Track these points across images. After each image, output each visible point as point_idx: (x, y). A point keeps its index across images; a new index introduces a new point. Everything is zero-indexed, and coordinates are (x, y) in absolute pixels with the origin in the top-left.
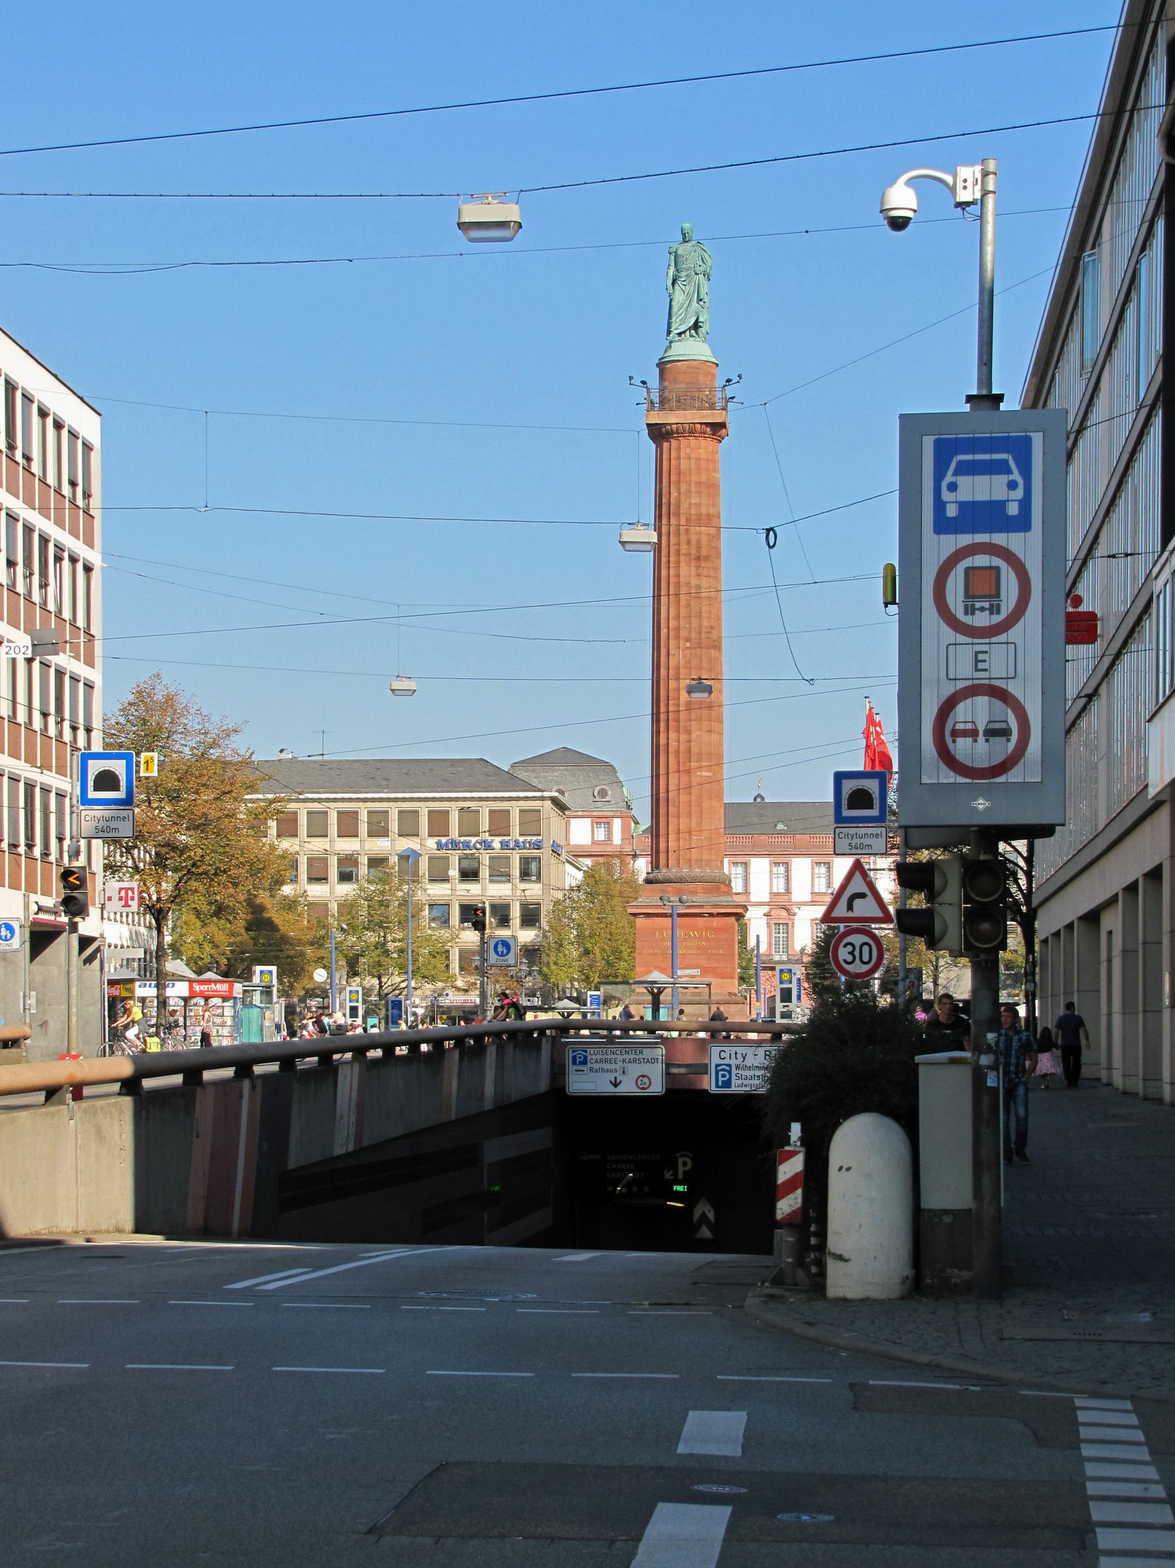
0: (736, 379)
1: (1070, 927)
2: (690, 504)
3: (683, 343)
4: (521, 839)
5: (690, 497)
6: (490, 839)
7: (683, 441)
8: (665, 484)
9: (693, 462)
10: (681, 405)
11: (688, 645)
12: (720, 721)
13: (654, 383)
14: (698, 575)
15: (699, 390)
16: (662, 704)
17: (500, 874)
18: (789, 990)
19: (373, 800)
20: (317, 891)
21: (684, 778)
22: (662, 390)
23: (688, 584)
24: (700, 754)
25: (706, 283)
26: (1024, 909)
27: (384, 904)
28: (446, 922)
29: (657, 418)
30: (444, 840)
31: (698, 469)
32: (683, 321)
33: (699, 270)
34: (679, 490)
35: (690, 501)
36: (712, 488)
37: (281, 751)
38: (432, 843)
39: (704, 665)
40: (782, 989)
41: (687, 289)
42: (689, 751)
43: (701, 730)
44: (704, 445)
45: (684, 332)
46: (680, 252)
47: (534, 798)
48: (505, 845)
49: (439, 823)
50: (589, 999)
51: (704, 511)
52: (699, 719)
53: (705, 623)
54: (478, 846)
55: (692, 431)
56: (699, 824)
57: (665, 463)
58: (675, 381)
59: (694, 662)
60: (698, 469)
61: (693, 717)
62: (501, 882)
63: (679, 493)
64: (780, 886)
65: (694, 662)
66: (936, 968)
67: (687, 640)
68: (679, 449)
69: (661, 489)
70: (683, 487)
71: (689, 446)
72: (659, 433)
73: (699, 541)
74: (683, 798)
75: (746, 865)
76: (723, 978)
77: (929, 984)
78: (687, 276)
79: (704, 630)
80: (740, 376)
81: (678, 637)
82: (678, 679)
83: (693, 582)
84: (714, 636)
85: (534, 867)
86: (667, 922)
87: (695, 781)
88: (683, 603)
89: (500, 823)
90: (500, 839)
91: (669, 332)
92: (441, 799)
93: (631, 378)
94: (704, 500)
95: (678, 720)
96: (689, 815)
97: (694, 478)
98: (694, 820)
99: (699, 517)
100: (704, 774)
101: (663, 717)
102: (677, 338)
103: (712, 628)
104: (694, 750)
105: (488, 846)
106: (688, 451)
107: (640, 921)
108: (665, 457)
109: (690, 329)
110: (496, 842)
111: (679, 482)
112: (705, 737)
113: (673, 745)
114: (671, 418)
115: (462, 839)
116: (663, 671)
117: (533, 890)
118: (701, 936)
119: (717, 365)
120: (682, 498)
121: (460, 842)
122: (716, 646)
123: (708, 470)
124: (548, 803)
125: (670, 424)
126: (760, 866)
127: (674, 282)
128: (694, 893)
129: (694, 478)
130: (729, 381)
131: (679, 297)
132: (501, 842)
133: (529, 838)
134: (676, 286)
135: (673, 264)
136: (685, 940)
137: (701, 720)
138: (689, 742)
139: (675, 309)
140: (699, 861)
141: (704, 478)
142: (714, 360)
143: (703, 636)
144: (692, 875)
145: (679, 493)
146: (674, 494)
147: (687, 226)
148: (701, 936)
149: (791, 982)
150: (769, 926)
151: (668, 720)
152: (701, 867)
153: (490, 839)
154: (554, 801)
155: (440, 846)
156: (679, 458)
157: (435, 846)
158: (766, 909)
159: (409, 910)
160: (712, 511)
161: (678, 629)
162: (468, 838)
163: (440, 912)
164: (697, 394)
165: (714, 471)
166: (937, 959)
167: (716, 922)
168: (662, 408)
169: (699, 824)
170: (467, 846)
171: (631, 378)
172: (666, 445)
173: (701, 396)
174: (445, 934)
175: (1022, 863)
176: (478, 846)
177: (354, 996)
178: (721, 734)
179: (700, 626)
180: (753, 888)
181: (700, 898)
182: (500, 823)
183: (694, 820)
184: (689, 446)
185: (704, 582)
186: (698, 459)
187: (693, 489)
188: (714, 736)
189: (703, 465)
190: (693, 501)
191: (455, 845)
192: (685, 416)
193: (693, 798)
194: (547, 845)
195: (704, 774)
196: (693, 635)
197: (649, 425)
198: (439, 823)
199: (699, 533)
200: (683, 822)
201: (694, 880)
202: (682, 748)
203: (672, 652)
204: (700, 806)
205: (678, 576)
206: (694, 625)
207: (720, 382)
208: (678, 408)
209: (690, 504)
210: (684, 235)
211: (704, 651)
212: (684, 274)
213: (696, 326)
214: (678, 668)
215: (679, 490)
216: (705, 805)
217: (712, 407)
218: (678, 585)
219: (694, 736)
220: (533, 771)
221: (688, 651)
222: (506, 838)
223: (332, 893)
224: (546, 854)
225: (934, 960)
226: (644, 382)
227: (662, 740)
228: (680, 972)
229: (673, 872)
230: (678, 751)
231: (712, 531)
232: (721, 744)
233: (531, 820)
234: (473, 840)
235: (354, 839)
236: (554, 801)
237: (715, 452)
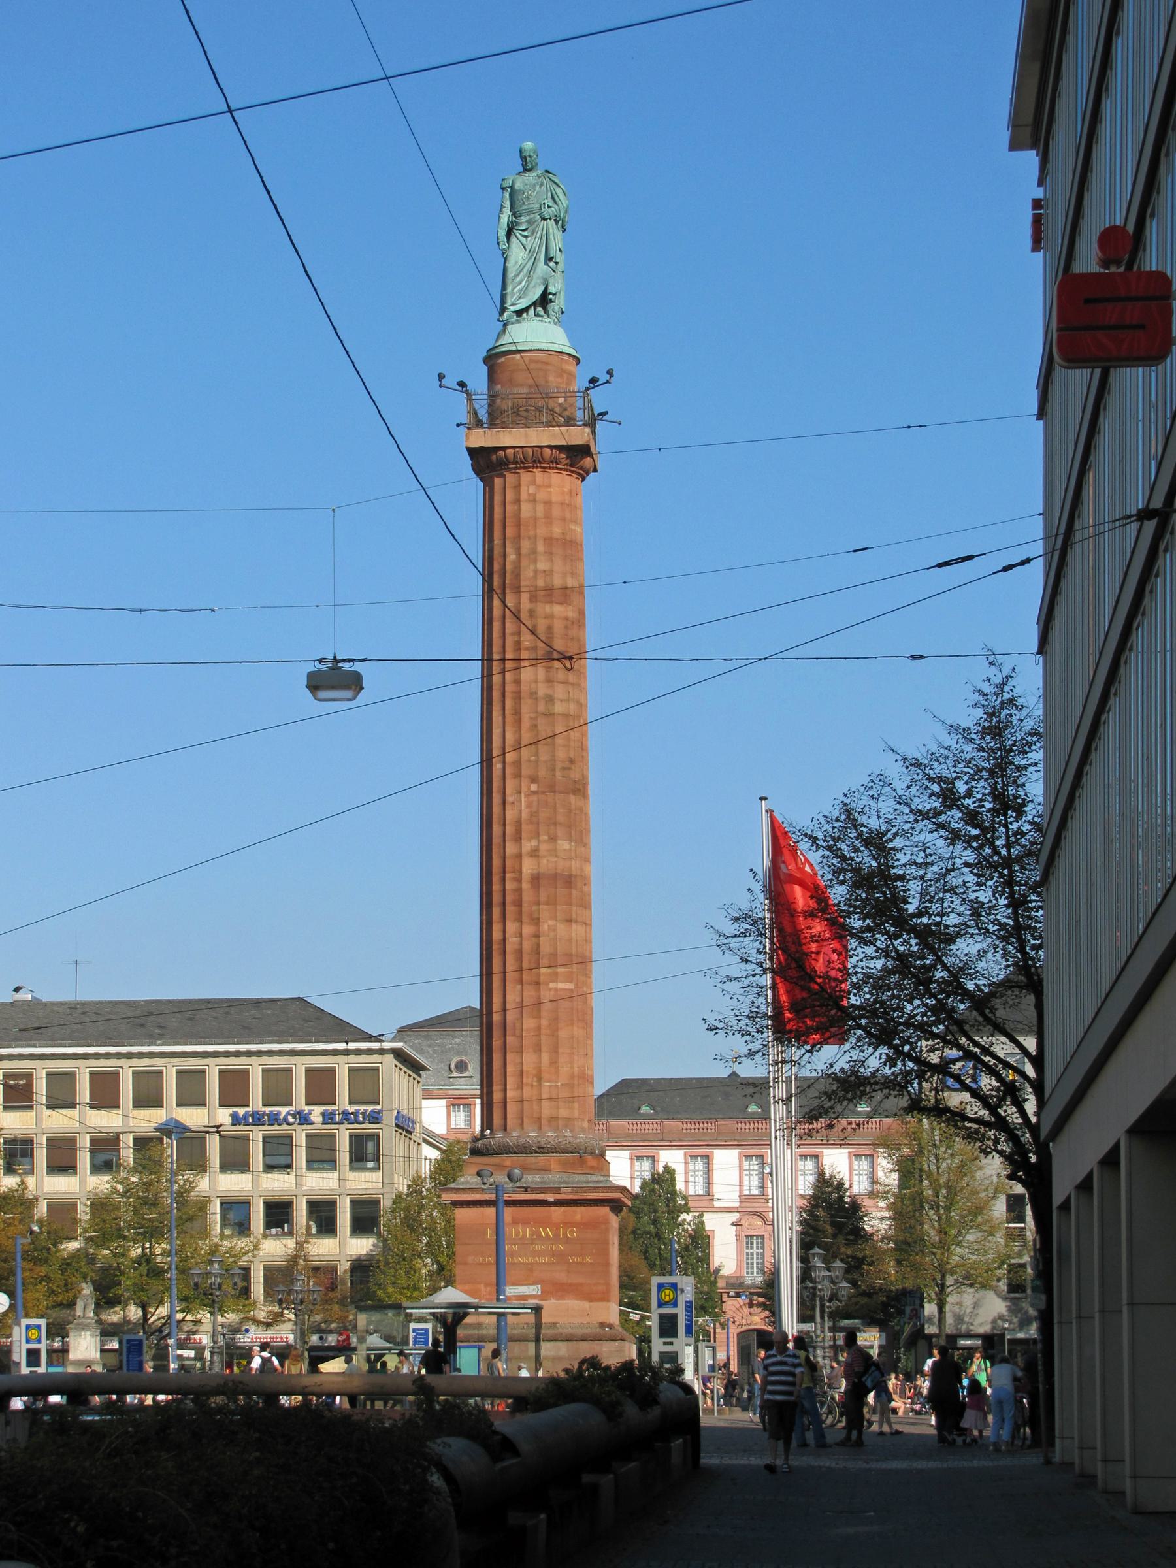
0: (603, 377)
1: (1110, 1160)
2: (536, 571)
3: (524, 325)
4: (352, 1109)
5: (535, 561)
6: (307, 1109)
7: (525, 477)
8: (497, 541)
9: (540, 508)
10: (521, 418)
11: (534, 787)
12: (586, 905)
13: (479, 381)
14: (549, 681)
15: (548, 396)
16: (496, 879)
17: (322, 1155)
18: (673, 1318)
19: (140, 1055)
20: (61, 1186)
21: (529, 994)
22: (493, 397)
23: (533, 695)
24: (554, 955)
25: (559, 234)
26: (1033, 1158)
27: (154, 1203)
28: (243, 1228)
29: (482, 439)
30: (241, 1111)
31: (548, 517)
32: (524, 293)
33: (547, 212)
34: (518, 551)
35: (538, 567)
36: (571, 548)
37: (17, 990)
38: (224, 1116)
39: (561, 818)
40: (661, 1316)
41: (529, 242)
42: (537, 950)
43: (555, 918)
44: (559, 483)
45: (526, 310)
46: (518, 186)
47: (370, 1052)
48: (328, 1118)
49: (234, 1088)
50: (411, 1335)
51: (557, 582)
52: (552, 902)
53: (561, 754)
54: (291, 1119)
55: (535, 459)
56: (554, 1063)
57: (497, 510)
58: (511, 382)
59: (543, 815)
60: (548, 517)
61: (543, 898)
62: (323, 1169)
63: (519, 555)
64: (752, 1185)
65: (543, 815)
66: (942, 1287)
67: (534, 780)
68: (517, 487)
69: (491, 550)
70: (525, 545)
71: (533, 483)
72: (487, 463)
73: (550, 628)
74: (529, 1023)
75: (707, 1159)
76: (591, 1300)
77: (930, 1309)
78: (528, 222)
79: (559, 765)
80: (610, 373)
81: (518, 776)
82: (518, 838)
83: (542, 690)
84: (575, 775)
85: (370, 1146)
86: (491, 1212)
87: (546, 995)
88: (526, 724)
89: (321, 1086)
90: (322, 1109)
91: (503, 310)
92: (238, 1054)
93: (441, 377)
94: (558, 565)
95: (519, 904)
96: (538, 1049)
97: (542, 531)
98: (545, 1057)
99: (550, 590)
100: (561, 985)
101: (496, 898)
102: (515, 318)
103: (572, 761)
104: (545, 949)
105: (304, 1119)
106: (532, 490)
107: (462, 1214)
108: (497, 498)
109: (534, 304)
110: (316, 1113)
111: (518, 538)
112: (562, 929)
113: (512, 942)
114: (509, 438)
115: (267, 1109)
116: (496, 828)
117: (366, 1182)
118: (556, 1235)
119: (578, 361)
120: (524, 563)
121: (264, 1114)
122: (579, 789)
123: (564, 519)
124: (390, 1059)
125: (504, 449)
126: (726, 1159)
127: (509, 234)
128: (546, 1170)
129: (542, 531)
130: (593, 381)
131: (517, 255)
132: (323, 1114)
133: (362, 1108)
134: (513, 239)
135: (507, 204)
136: (532, 1242)
137: (555, 904)
138: (537, 936)
139: (511, 274)
140: (554, 1119)
141: (557, 530)
142: (572, 352)
143: (558, 774)
144: (543, 1141)
145: (519, 555)
146: (511, 557)
147: (528, 146)
148: (556, 1235)
149: (675, 1305)
150: (739, 1240)
151: (504, 904)
152: (557, 1129)
153: (307, 1109)
154: (399, 1054)
155: (236, 1119)
156: (518, 501)
157: (229, 1120)
158: (735, 1217)
159: (192, 1212)
160: (570, 582)
161: (518, 763)
162: (278, 1108)
163: (236, 1212)
164: (541, 403)
165: (574, 521)
166: (943, 1276)
167: (579, 1213)
168: (492, 425)
169: (554, 1063)
170: (274, 1119)
171: (441, 377)
172: (498, 482)
173: (551, 404)
174: (241, 1244)
175: (1030, 1071)
176: (291, 1119)
177: (34, 1334)
178: (587, 924)
179: (553, 759)
180: (718, 1191)
181: (555, 1176)
182: (321, 1086)
183: (545, 1057)
184: (533, 483)
185: (559, 691)
186: (548, 503)
187: (541, 548)
188: (577, 929)
189: (556, 512)
190: (541, 566)
191: (257, 1119)
192: (526, 435)
193: (544, 1022)
194: (389, 1119)
195: (561, 985)
196: (543, 773)
197: (473, 452)
198: (234, 1088)
199: (551, 617)
200: (529, 1059)
201: (542, 1150)
202: (527, 945)
203: (509, 799)
204: (554, 1033)
205: (517, 682)
206: (544, 757)
207: (581, 383)
208: (517, 424)
209: (536, 571)
210: (523, 158)
211: (559, 796)
212: (524, 219)
213: (544, 300)
214: (519, 823)
215: (518, 551)
216: (563, 1034)
217: (570, 422)
218: (518, 696)
219: (545, 927)
220: (427, 1037)
221: (535, 798)
222: (330, 1108)
223: (82, 1185)
224: (387, 1131)
225: (938, 1277)
226: (462, 384)
227: (496, 935)
228: (510, 1291)
229: (514, 1136)
230: (519, 953)
231: (571, 613)
232: (587, 940)
233: (366, 1083)
234: (283, 1110)
235: (115, 1111)
236: (399, 1054)
237: (573, 493)
